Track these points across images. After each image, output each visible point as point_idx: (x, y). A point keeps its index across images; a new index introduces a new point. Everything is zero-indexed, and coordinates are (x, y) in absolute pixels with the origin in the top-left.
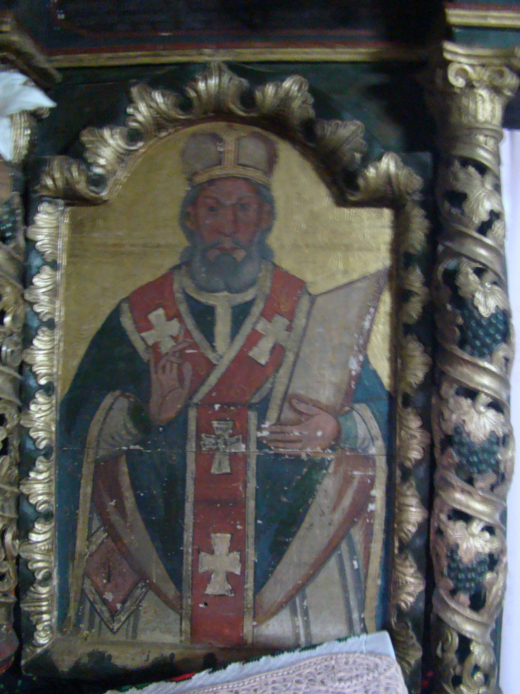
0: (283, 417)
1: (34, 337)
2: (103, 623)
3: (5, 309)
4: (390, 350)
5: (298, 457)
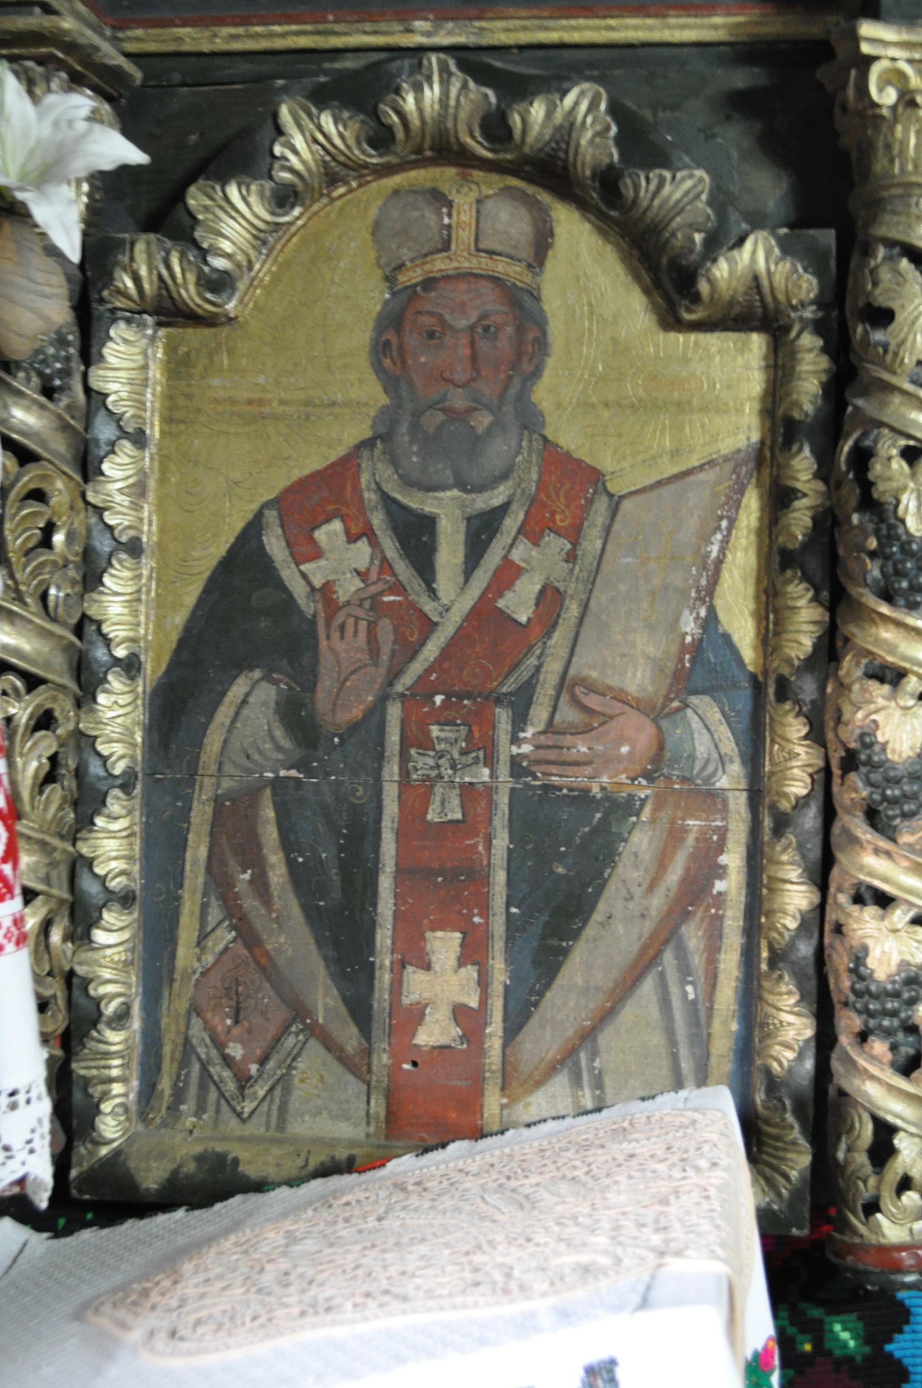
0: (558, 718)
1: (105, 571)
2: (223, 1101)
3: (55, 519)
4: (757, 598)
5: (586, 791)
